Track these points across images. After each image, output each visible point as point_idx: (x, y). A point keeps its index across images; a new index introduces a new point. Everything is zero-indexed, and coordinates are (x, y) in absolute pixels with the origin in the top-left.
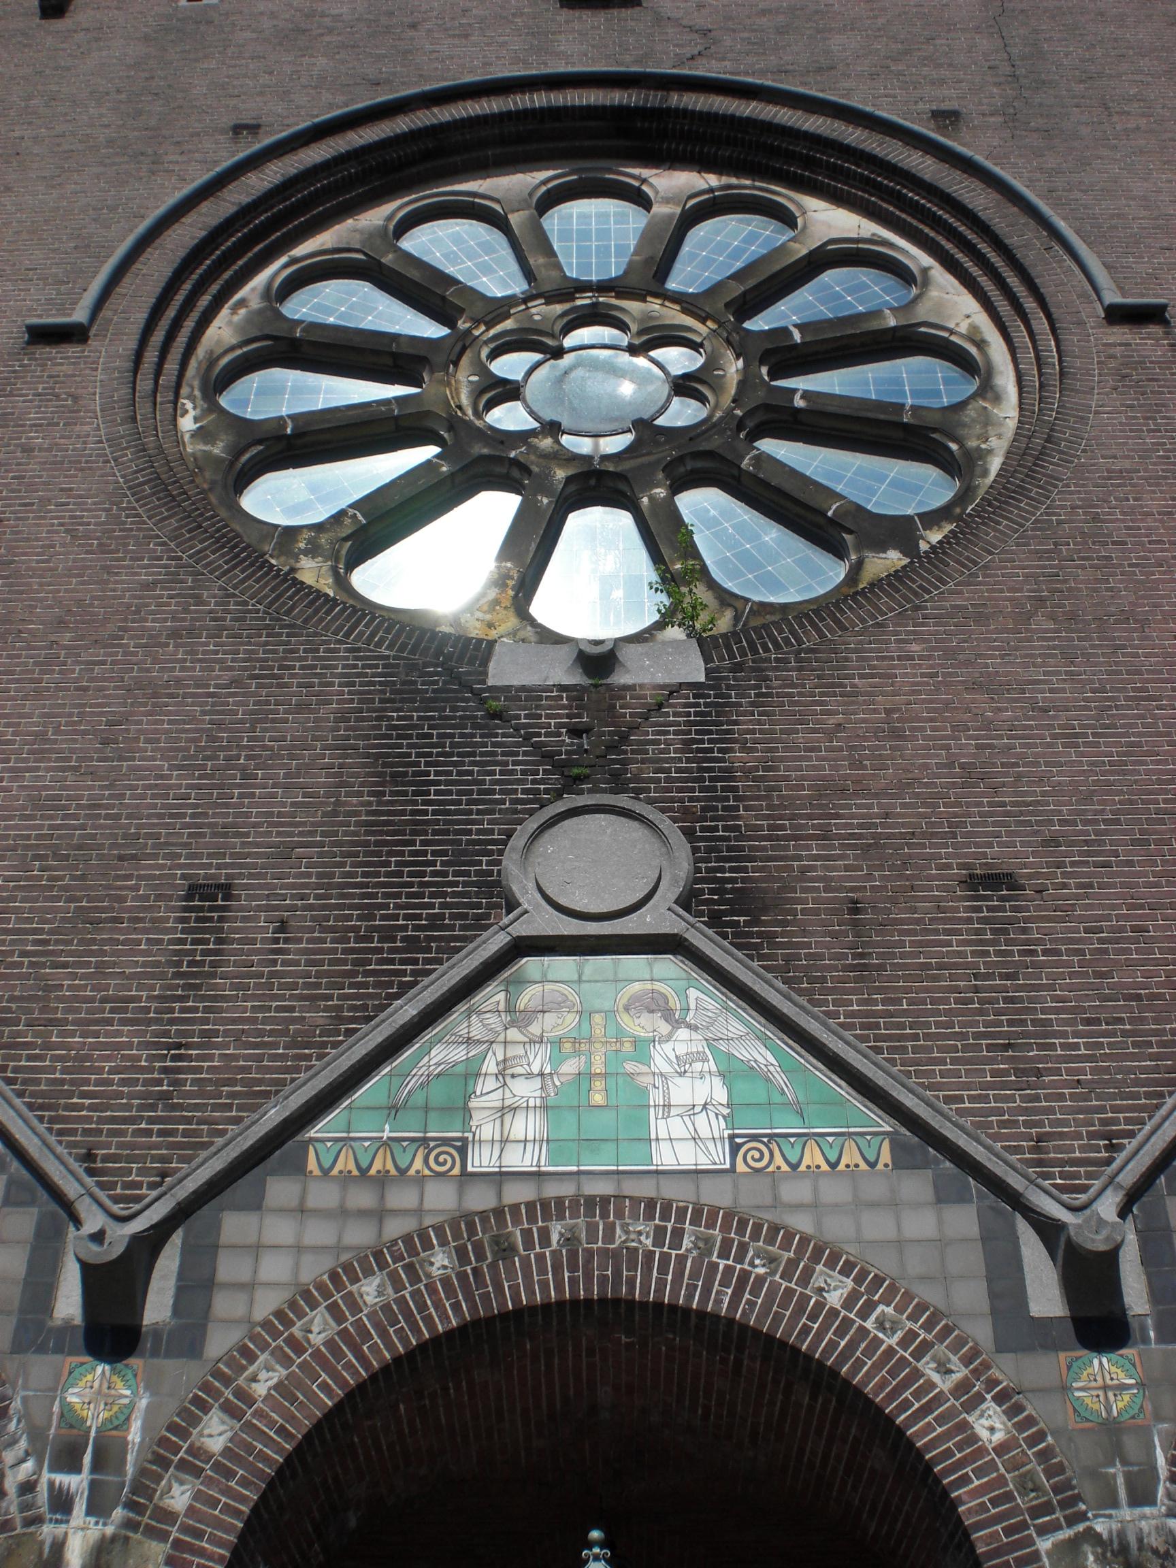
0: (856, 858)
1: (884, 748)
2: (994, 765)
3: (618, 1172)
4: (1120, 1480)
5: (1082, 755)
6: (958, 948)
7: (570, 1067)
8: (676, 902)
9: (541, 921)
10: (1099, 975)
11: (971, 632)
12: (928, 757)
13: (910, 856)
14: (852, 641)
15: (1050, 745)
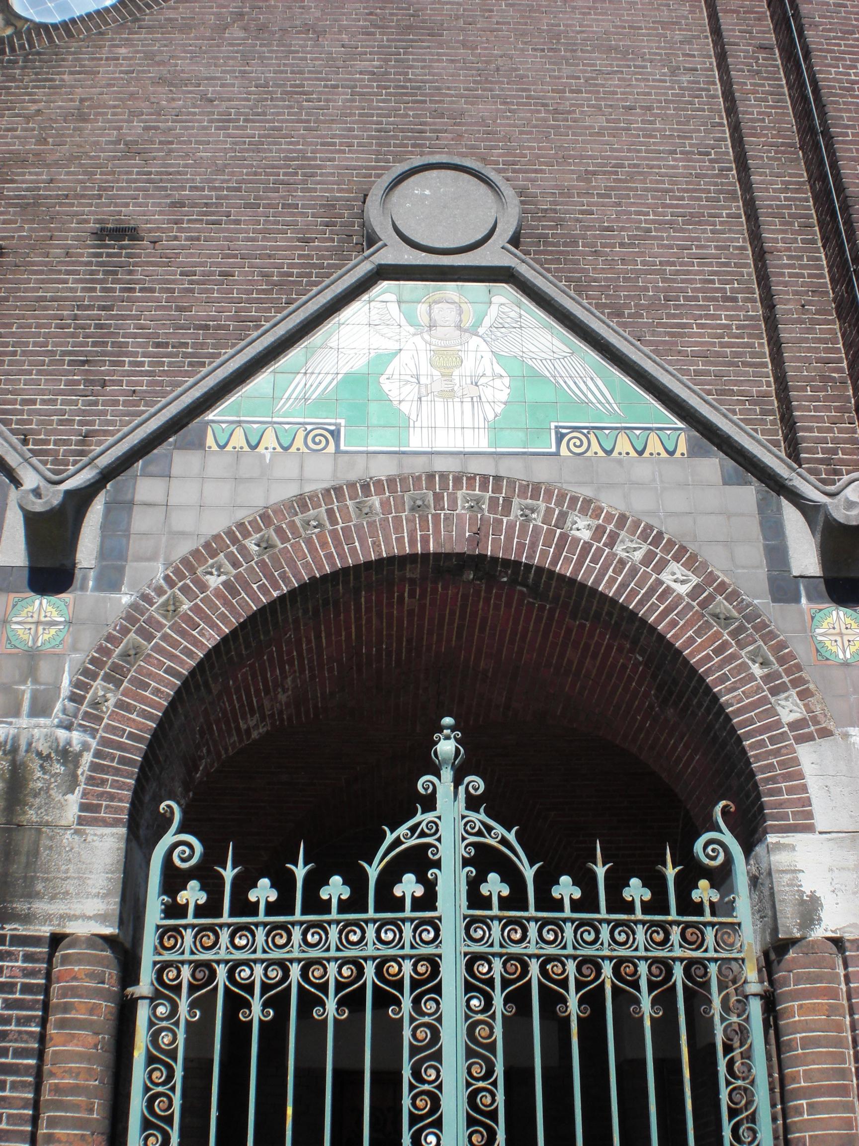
0: (15, 214)
1: (68, 128)
2: (153, 143)
3: (368, 453)
4: (27, 696)
5: (229, 136)
6: (74, 286)
8: (509, 242)
10: (180, 309)
11: (171, 40)
12: (101, 136)
13: (58, 213)
14: (74, 46)
15: (205, 128)
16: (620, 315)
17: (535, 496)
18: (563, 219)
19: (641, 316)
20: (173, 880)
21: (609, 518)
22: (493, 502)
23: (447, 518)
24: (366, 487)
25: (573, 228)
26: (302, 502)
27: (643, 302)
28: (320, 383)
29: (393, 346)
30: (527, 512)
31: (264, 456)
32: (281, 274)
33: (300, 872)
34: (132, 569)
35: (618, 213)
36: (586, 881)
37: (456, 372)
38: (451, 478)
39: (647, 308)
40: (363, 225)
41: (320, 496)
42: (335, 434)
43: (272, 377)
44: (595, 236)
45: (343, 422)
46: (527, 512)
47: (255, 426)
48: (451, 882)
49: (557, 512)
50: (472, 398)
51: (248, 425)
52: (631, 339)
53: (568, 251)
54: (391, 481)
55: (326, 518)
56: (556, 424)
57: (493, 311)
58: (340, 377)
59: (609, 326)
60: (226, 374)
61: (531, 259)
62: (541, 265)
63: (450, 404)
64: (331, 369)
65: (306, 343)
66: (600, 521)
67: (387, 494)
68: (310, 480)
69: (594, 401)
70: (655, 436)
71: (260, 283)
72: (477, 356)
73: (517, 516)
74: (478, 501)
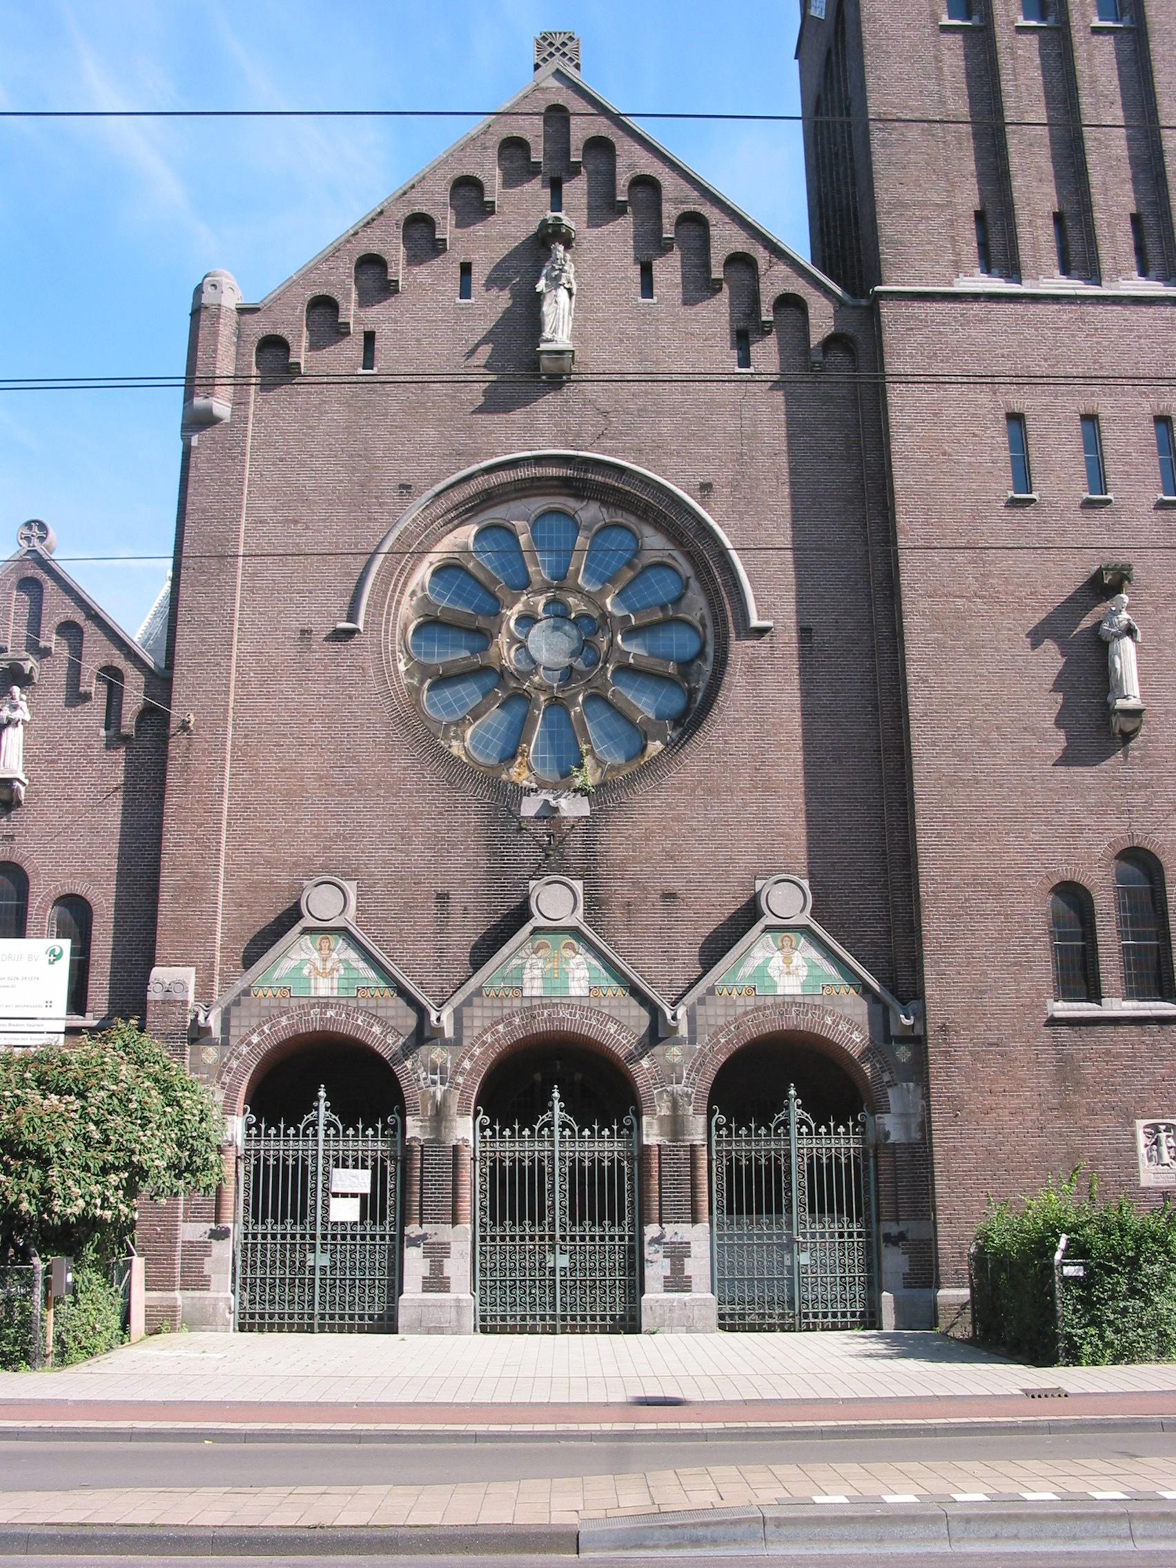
7: (548, 966)
20: (719, 1128)
33: (282, 1126)
34: (699, 1038)
36: (828, 1127)
48: (321, 1128)
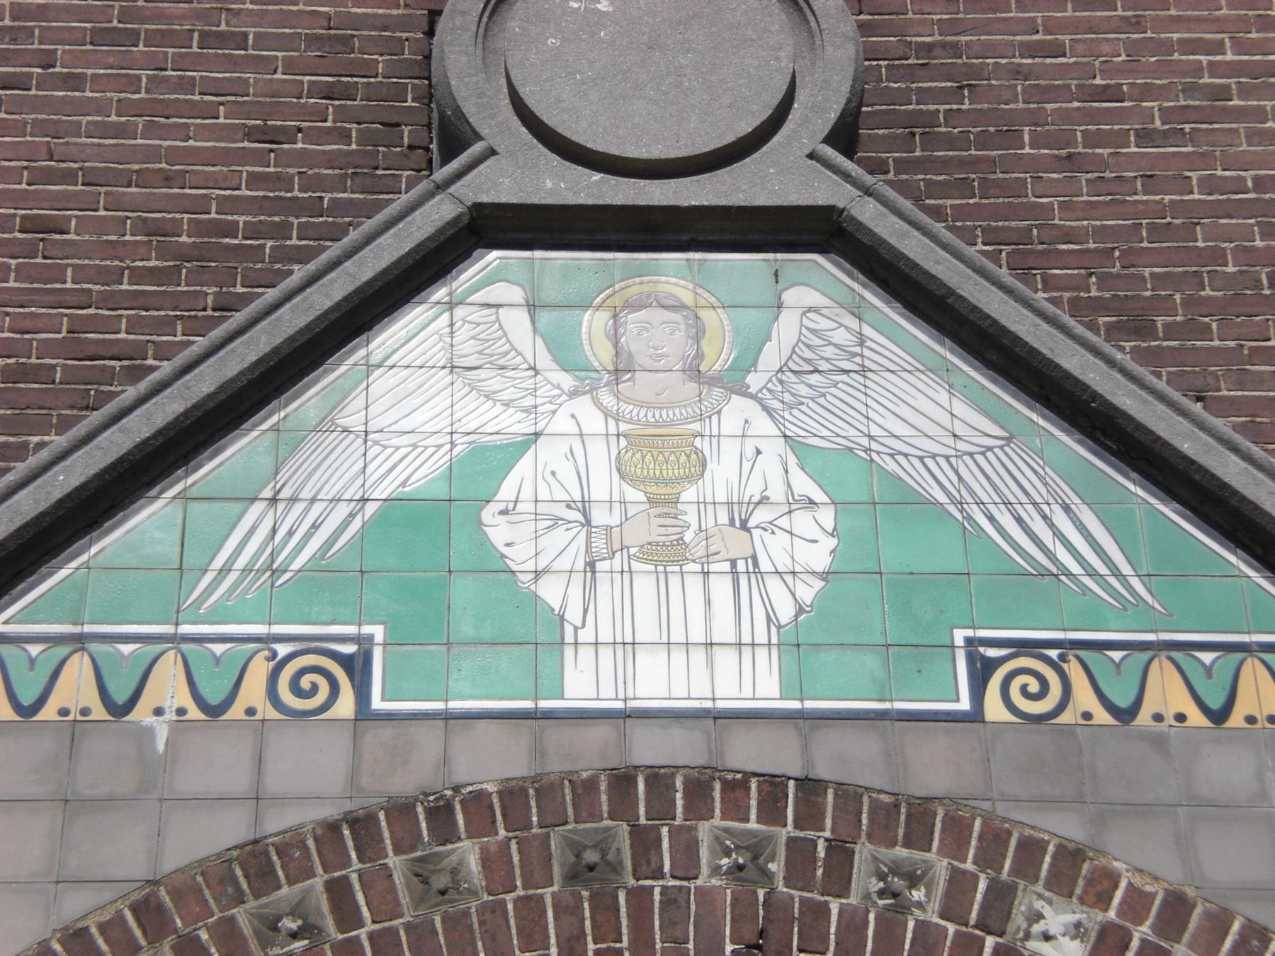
3: (448, 717)
8: (828, 140)
9: (516, 175)
16: (1143, 330)
17: (918, 838)
18: (977, 72)
19: (1205, 332)
21: (1136, 903)
22: (800, 852)
23: (670, 899)
24: (441, 814)
25: (1007, 95)
26: (257, 863)
27: (1208, 292)
28: (315, 526)
29: (515, 424)
30: (897, 883)
31: (150, 732)
32: (199, 229)
35: (1133, 49)
37: (689, 494)
38: (679, 783)
39: (1221, 308)
40: (428, 96)
41: (311, 843)
42: (357, 667)
43: (175, 512)
44: (1067, 116)
45: (378, 632)
46: (897, 883)
47: (126, 649)
49: (982, 885)
50: (734, 563)
51: (105, 648)
52: (1177, 396)
53: (992, 161)
54: (513, 794)
55: (325, 906)
56: (970, 633)
57: (787, 329)
58: (370, 508)
59: (1111, 363)
60: (43, 506)
61: (890, 183)
62: (917, 200)
63: (675, 581)
64: (346, 487)
65: (275, 418)
66: (1112, 914)
67: (502, 833)
68: (282, 800)
69: (1075, 568)
70: (1257, 662)
71: (142, 250)
72: (743, 453)
73: (867, 896)
74: (757, 849)
